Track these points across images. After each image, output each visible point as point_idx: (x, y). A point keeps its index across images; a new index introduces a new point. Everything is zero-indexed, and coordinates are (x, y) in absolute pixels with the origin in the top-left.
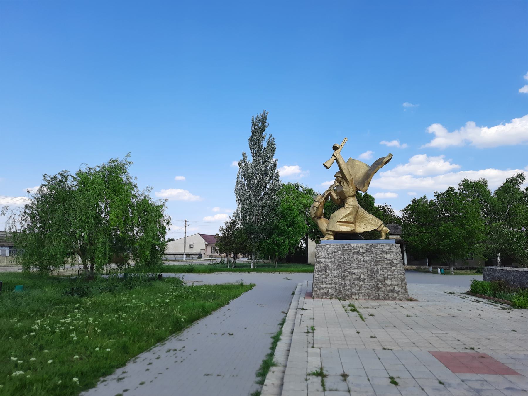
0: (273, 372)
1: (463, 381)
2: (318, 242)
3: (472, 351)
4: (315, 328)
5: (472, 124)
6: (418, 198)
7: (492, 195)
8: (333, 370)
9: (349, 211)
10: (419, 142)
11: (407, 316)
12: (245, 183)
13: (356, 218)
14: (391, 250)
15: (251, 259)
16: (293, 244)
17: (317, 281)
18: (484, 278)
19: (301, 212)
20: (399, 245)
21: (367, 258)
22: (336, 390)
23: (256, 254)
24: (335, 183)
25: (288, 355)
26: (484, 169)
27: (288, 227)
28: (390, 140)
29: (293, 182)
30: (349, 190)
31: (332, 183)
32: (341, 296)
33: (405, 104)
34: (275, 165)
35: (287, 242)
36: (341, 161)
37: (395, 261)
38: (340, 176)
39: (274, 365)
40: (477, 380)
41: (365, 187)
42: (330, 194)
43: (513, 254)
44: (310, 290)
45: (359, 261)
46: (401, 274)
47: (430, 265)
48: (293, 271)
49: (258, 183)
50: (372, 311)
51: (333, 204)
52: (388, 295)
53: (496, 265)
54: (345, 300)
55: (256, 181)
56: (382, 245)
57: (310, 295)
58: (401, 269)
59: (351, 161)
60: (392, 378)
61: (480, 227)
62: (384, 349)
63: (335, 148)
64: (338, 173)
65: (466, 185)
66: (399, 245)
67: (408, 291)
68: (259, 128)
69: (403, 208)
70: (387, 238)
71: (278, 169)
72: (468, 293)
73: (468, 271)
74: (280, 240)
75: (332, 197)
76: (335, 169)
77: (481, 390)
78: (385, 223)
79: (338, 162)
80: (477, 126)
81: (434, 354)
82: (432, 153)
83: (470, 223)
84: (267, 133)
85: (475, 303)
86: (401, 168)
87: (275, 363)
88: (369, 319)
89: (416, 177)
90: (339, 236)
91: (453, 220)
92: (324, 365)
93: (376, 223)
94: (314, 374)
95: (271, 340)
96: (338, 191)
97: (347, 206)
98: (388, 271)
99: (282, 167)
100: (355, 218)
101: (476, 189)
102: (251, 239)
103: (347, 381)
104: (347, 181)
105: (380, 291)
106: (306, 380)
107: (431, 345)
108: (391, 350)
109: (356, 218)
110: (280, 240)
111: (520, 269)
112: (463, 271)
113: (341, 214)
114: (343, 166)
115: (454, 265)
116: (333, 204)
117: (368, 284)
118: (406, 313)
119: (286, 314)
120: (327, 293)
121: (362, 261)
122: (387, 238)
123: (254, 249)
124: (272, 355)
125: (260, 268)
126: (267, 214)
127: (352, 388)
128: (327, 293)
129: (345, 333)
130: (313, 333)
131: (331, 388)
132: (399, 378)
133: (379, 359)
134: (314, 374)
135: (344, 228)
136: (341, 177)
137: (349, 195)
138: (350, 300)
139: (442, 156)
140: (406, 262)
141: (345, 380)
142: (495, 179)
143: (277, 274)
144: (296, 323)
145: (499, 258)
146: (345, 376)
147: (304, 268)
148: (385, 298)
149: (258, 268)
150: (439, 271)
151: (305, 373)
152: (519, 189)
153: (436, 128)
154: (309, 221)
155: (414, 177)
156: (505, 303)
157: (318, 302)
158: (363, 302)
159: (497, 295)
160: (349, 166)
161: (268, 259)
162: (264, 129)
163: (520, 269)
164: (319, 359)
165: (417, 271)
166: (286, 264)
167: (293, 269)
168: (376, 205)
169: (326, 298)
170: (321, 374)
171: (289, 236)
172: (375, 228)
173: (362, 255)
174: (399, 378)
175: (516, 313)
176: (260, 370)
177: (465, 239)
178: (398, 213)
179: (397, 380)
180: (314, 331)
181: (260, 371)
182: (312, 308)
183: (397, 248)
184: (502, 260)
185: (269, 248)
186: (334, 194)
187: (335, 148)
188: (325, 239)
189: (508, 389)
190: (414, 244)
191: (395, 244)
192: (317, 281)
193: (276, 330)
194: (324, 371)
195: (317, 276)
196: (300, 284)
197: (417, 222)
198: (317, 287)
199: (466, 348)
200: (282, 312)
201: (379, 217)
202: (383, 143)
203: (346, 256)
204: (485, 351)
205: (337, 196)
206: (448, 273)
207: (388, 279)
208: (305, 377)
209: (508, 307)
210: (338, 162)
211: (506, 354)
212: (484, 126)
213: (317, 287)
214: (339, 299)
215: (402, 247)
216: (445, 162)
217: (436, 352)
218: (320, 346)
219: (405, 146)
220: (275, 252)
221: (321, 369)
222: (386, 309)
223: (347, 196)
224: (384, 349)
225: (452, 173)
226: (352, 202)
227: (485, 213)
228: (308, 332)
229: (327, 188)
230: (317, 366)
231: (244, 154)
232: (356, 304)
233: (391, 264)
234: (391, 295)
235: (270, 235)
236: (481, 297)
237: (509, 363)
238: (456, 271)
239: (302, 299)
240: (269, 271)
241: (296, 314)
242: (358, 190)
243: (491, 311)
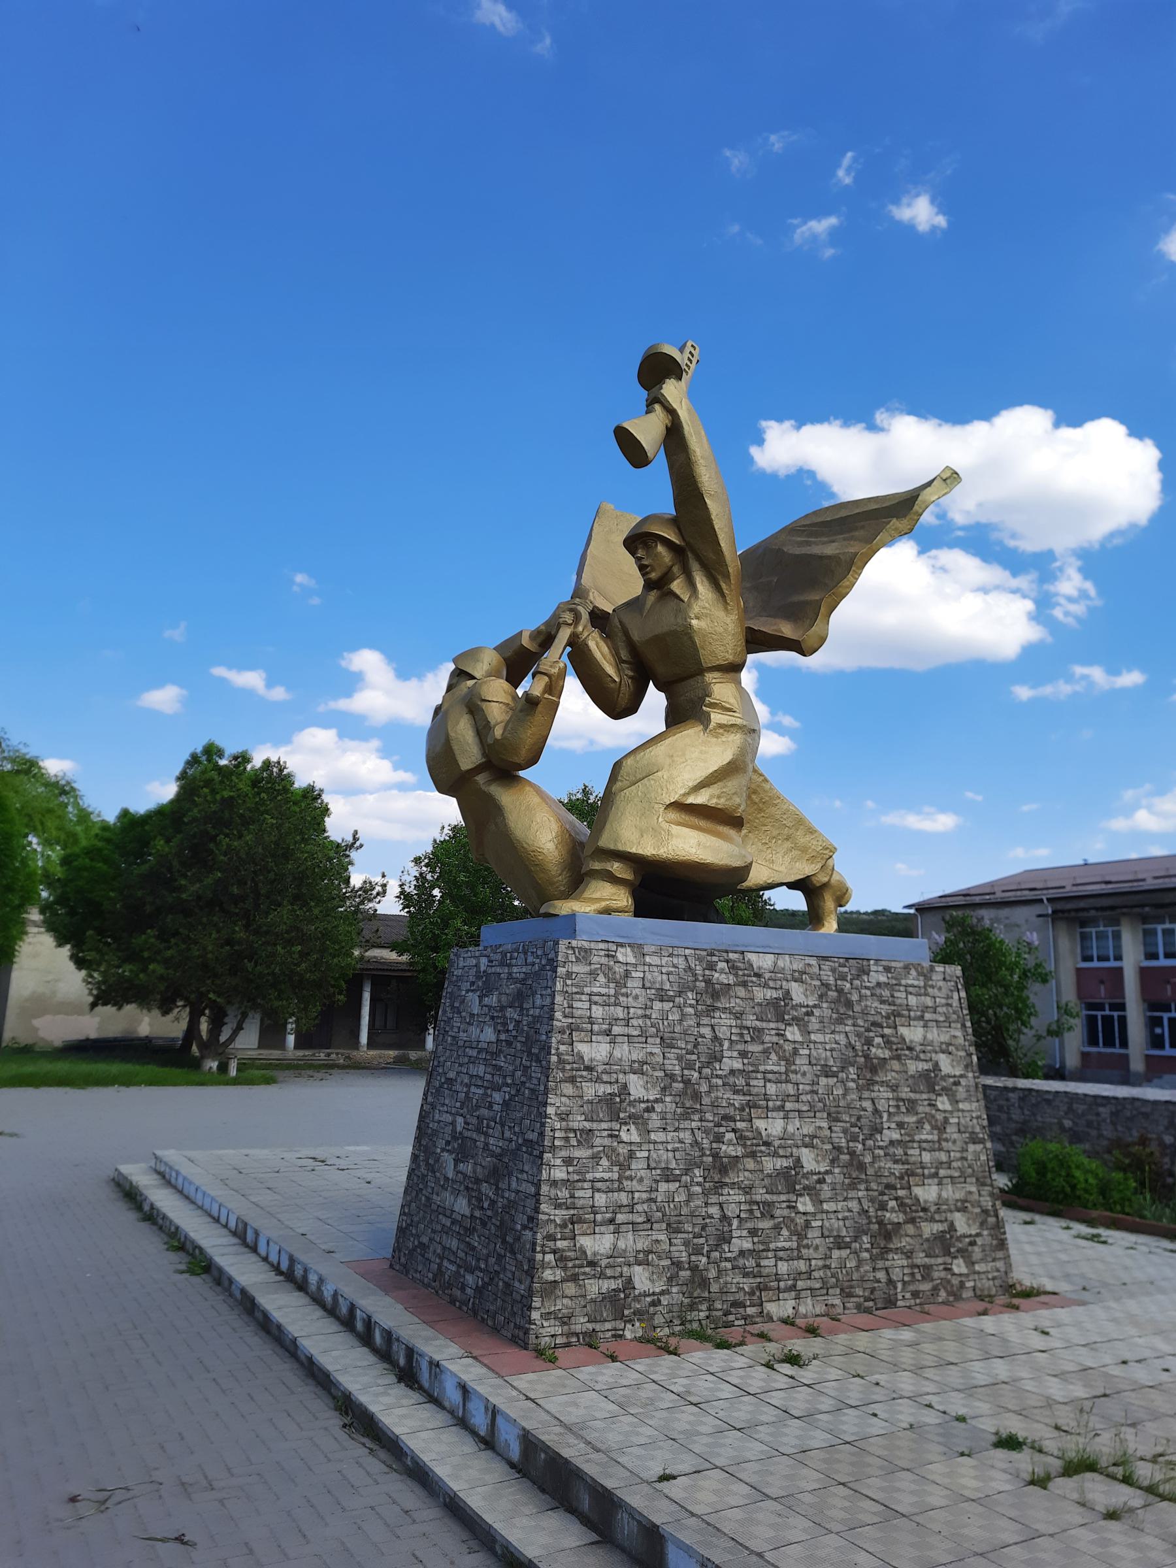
20: (957, 970)
56: (887, 969)
66: (957, 970)
120: (618, 1303)
128: (618, 1303)
139: (375, 743)
195: (559, 1174)
202: (220, 671)
203: (725, 1024)
219: (279, 694)
223: (707, 660)
225: (395, 792)
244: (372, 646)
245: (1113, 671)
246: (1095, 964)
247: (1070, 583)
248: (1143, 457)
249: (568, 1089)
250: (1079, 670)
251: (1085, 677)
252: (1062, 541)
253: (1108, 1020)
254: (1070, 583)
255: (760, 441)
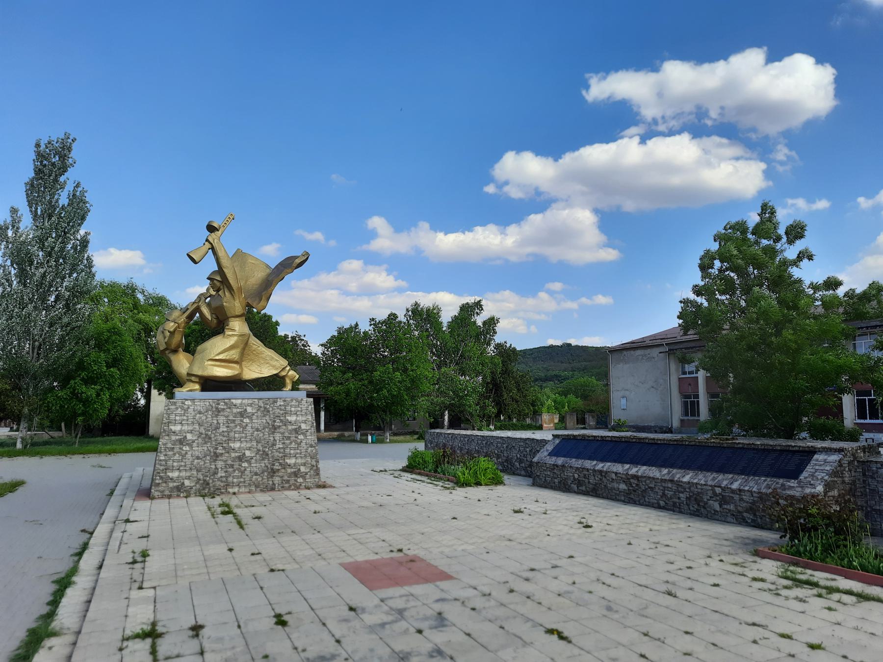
0: (50, 648)
1: (382, 601)
2: (170, 396)
3: (400, 554)
4: (150, 553)
5: (425, 225)
6: (347, 326)
7: (444, 329)
8: (174, 621)
9: (232, 341)
10: (353, 242)
11: (315, 512)
12: (13, 272)
13: (244, 353)
14: (298, 407)
15: (17, 430)
16: (118, 400)
17: (161, 468)
18: (426, 446)
19: (138, 339)
20: (312, 400)
21: (257, 422)
22: (178, 656)
23: (31, 420)
24: (208, 290)
25: (87, 611)
26: (437, 292)
27: (108, 367)
28: (311, 231)
29: (123, 280)
30: (235, 305)
31: (203, 290)
32: (206, 490)
33: (334, 176)
34: (85, 243)
35: (106, 396)
36: (221, 254)
37: (303, 426)
38: (219, 278)
39: (54, 634)
40: (401, 596)
41: (262, 303)
42: (198, 309)
43: (462, 412)
44: (146, 484)
45: (244, 428)
46: (311, 446)
47: (357, 431)
48: (115, 452)
49: (44, 276)
50: (257, 511)
51: (201, 329)
52: (288, 482)
53: (443, 428)
54: (213, 497)
55: (42, 270)
56: (284, 401)
57: (146, 494)
58: (312, 438)
59: (239, 255)
60: (278, 616)
61: (427, 373)
62: (272, 570)
63: (211, 229)
64: (214, 272)
65: (416, 311)
66: (312, 400)
67: (321, 472)
68: (53, 164)
69: (324, 341)
70: (294, 388)
71: (90, 251)
72: (404, 470)
73: (408, 437)
74: (90, 392)
75: (201, 314)
76: (209, 265)
77: (405, 609)
78: (293, 365)
79: (215, 253)
80: (431, 229)
81: (347, 567)
82: (373, 260)
83: (414, 367)
84: (70, 178)
85: (411, 484)
86: (325, 278)
87: (57, 629)
88: (253, 526)
89: (347, 293)
90: (210, 384)
91: (393, 361)
92: (159, 616)
93: (278, 364)
94: (137, 636)
95: (54, 587)
96: (213, 305)
97: (228, 333)
98: (291, 443)
99: (105, 248)
100: (242, 354)
101: (425, 317)
102: (20, 390)
103: (200, 637)
104: (230, 288)
105: (276, 476)
106: (121, 649)
107: (343, 554)
108: (283, 570)
109: (244, 353)
110: (90, 392)
111: (469, 432)
112: (401, 438)
113: (217, 346)
114: (225, 262)
115: (391, 429)
116: (201, 329)
117: (256, 466)
118: (314, 507)
119: (92, 533)
121: (249, 428)
122: (294, 388)
123: (26, 410)
124: (50, 616)
125: (37, 449)
126: (62, 338)
127: (207, 646)
129: (206, 553)
130: (144, 562)
131: (169, 654)
132: (290, 613)
133: (262, 588)
134: (137, 636)
135: (221, 372)
136: (220, 281)
137: (233, 314)
138: (223, 496)
139: (385, 266)
140: (322, 427)
141: (197, 635)
142: (448, 304)
143: (77, 458)
144: (109, 547)
145: (446, 418)
146: (196, 629)
147: (140, 445)
148: (283, 487)
149: (33, 448)
150: (370, 438)
151: (120, 637)
152: (475, 322)
153: (377, 222)
154: (156, 356)
155: (343, 294)
156: (448, 480)
157: (161, 505)
158: (245, 498)
159: (439, 470)
160: (235, 264)
161: (61, 430)
162: (64, 169)
163: (469, 432)
164: (152, 607)
165: (339, 439)
166: (99, 439)
167: (114, 447)
168: (281, 332)
169: (178, 496)
170: (152, 634)
171: (109, 384)
172: (275, 372)
173: (250, 418)
174: (290, 613)
175: (460, 493)
176: (18, 649)
177: (408, 389)
178: (316, 349)
179: (285, 618)
180: (147, 559)
181: (20, 651)
182: (147, 518)
183: (308, 404)
184: (450, 421)
185: (62, 407)
186: (205, 311)
187: (211, 229)
188: (184, 390)
189: (438, 601)
190: (337, 398)
191: (305, 399)
192: (161, 468)
193: (63, 568)
194: (157, 628)
195: (162, 458)
196: (126, 475)
197: (344, 363)
198: (161, 478)
199: (392, 551)
200: (83, 531)
201: (284, 355)
202: (299, 232)
204: (416, 552)
205: (212, 314)
206: (382, 441)
207: (290, 456)
208: (119, 644)
209: (451, 485)
210: (215, 253)
211: (442, 553)
212: (441, 231)
213: (161, 478)
214: (203, 496)
215: (317, 403)
216: (388, 275)
217: (350, 563)
218: (154, 585)
219: (333, 243)
220: (75, 415)
221: (154, 624)
222: (283, 505)
223: (229, 314)
224: (272, 570)
225: (396, 293)
226: (238, 326)
227: (434, 354)
228: (134, 562)
229: (194, 298)
230: (145, 621)
231: (14, 211)
232: (234, 501)
233: (297, 431)
234: (294, 481)
235: (65, 382)
236: (419, 474)
237: (442, 564)
238: (392, 438)
239: (127, 502)
240: (60, 454)
241: (112, 532)
242: (249, 306)
243: (430, 493)
244: (380, 214)
245: (811, 200)
246: (688, 376)
247: (782, 153)
248: (825, 75)
249: (167, 438)
250: (790, 201)
251: (793, 205)
252: (772, 129)
253: (692, 403)
254: (782, 153)
255: (588, 87)
